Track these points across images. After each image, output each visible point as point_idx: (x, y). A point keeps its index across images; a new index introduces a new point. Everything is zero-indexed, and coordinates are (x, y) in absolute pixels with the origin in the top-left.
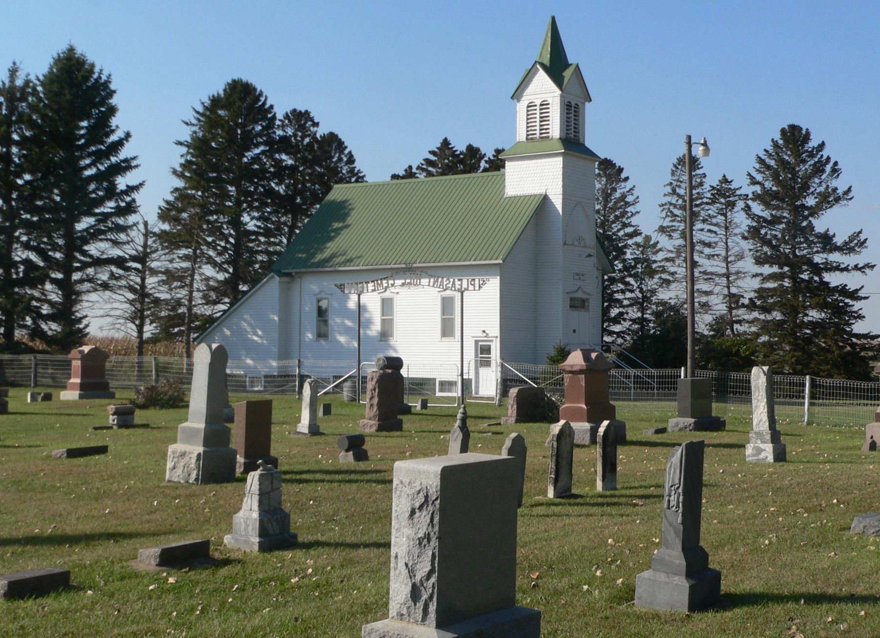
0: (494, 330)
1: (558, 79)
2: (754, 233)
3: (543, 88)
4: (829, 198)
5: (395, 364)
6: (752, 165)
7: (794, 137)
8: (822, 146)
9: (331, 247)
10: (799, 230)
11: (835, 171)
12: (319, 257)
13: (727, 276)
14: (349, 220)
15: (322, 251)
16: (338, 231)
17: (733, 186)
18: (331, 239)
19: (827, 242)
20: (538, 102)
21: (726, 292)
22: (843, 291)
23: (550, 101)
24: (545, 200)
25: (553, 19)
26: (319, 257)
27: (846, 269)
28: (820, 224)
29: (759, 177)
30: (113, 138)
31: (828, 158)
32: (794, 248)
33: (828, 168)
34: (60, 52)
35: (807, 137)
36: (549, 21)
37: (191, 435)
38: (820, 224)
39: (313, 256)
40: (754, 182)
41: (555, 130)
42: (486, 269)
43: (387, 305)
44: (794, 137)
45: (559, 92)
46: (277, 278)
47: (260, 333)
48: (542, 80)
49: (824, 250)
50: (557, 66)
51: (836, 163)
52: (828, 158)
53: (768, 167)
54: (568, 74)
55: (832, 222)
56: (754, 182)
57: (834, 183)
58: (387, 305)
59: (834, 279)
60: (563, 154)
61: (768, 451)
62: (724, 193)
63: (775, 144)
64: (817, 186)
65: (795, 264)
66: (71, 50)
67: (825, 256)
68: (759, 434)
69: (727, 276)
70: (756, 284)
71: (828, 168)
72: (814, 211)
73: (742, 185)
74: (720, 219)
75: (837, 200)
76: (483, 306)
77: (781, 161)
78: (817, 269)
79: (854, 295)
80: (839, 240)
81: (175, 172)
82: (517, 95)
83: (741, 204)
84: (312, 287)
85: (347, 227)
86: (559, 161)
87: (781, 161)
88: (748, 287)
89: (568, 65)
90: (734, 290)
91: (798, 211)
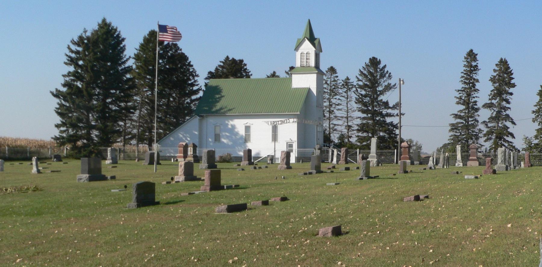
0: (295, 138)
1: (314, 45)
2: (358, 101)
3: (307, 47)
4: (388, 88)
5: (250, 151)
6: (357, 73)
7: (374, 62)
8: (385, 66)
9: (218, 106)
10: (374, 100)
11: (390, 76)
12: (214, 109)
13: (347, 118)
14: (223, 94)
15: (215, 106)
16: (220, 98)
17: (351, 81)
18: (218, 102)
19: (386, 105)
20: (305, 53)
21: (346, 124)
22: (391, 124)
23: (310, 52)
24: (309, 90)
25: (472, 56)
26: (214, 109)
27: (393, 116)
28: (383, 98)
29: (360, 78)
30: (125, 59)
31: (387, 71)
32: (373, 107)
33: (387, 75)
34: (112, 25)
35: (379, 62)
36: (308, 21)
37: (373, 157)
38: (383, 98)
39: (212, 108)
40: (359, 80)
41: (312, 63)
42: (293, 116)
43: (247, 128)
44: (374, 62)
45: (314, 49)
46: (198, 118)
47: (189, 139)
48: (307, 43)
49: (385, 108)
50: (312, 39)
51: (390, 73)
52: (387, 71)
53: (365, 75)
54: (316, 42)
55: (390, 97)
56: (359, 80)
57: (390, 81)
58: (247, 128)
59: (388, 120)
60: (317, 73)
61: (461, 164)
62: (347, 83)
63: (367, 65)
64: (384, 82)
65: (375, 113)
66: (104, 21)
67: (386, 110)
68: (459, 161)
69: (347, 118)
70: (359, 122)
71: (387, 75)
72: (382, 93)
73: (353, 80)
74: (344, 94)
75: (391, 88)
76: (289, 131)
77: (370, 73)
78: (383, 116)
79: (396, 126)
80: (391, 105)
81: (66, 63)
82: (297, 49)
83: (354, 89)
84: (211, 121)
85: (223, 96)
86: (315, 75)
87: (370, 73)
88: (356, 123)
89: (316, 39)
90: (350, 124)
91: (375, 92)
